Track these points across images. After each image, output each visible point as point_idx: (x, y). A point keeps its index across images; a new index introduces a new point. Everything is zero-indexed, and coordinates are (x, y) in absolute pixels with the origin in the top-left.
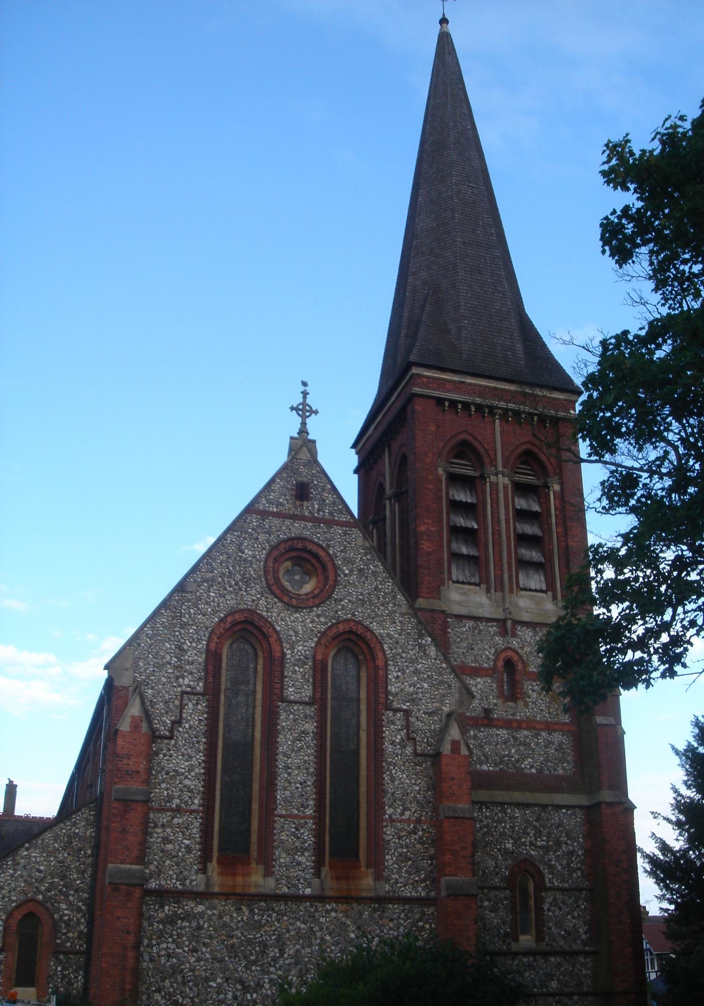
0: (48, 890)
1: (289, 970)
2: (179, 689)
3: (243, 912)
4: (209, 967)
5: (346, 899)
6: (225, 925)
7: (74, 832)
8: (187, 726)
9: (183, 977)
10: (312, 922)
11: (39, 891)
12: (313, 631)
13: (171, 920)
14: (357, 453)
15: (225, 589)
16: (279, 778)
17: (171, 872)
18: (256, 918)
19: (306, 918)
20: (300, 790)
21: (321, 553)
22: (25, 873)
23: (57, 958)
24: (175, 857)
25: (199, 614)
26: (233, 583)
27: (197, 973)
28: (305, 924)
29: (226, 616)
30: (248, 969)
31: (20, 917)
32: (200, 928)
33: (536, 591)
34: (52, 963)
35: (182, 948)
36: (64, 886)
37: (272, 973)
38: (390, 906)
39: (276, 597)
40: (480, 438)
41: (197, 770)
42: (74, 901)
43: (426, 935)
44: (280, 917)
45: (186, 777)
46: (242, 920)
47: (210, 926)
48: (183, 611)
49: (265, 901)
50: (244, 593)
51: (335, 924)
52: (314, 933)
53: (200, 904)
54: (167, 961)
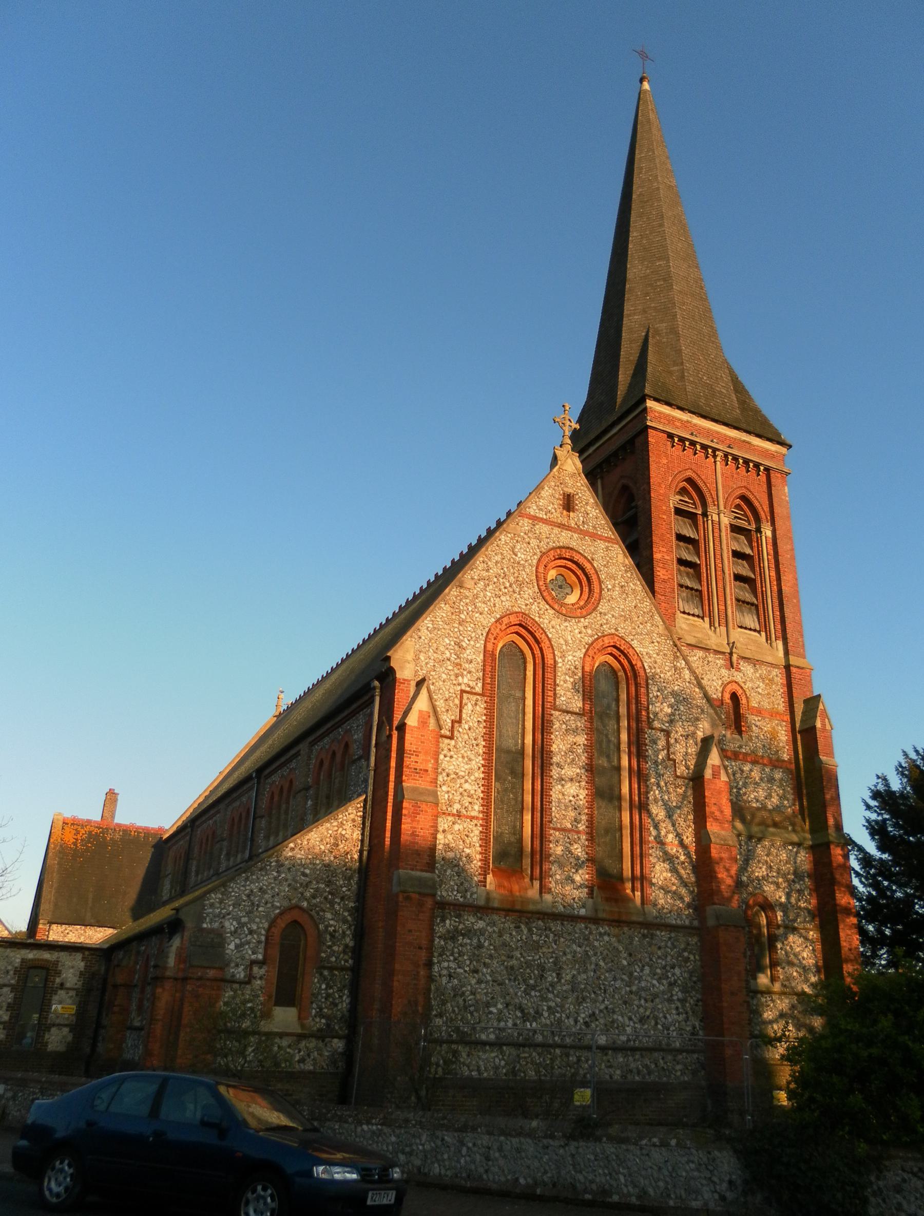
0: (314, 897)
1: (567, 998)
2: (459, 688)
3: (522, 931)
4: (490, 991)
5: (617, 922)
6: (505, 944)
7: (340, 834)
8: (467, 727)
9: (464, 1000)
10: (587, 946)
11: (303, 897)
12: (581, 641)
13: (452, 936)
15: (500, 590)
16: (553, 790)
17: (452, 883)
18: (535, 937)
19: (581, 941)
20: (573, 803)
21: (587, 566)
22: (289, 876)
23: (321, 974)
24: (456, 866)
25: (477, 613)
26: (508, 585)
27: (478, 997)
28: (580, 947)
29: (502, 617)
30: (528, 994)
31: (283, 926)
32: (480, 946)
33: (750, 629)
34: (316, 980)
35: (463, 968)
36: (330, 893)
37: (550, 1000)
38: (658, 933)
39: (548, 603)
40: (703, 477)
41: (477, 775)
42: (339, 911)
43: (691, 967)
44: (557, 938)
45: (466, 781)
46: (522, 939)
47: (491, 944)
48: (461, 608)
49: (542, 920)
50: (518, 596)
51: (608, 949)
52: (589, 957)
53: (481, 919)
54: (448, 982)
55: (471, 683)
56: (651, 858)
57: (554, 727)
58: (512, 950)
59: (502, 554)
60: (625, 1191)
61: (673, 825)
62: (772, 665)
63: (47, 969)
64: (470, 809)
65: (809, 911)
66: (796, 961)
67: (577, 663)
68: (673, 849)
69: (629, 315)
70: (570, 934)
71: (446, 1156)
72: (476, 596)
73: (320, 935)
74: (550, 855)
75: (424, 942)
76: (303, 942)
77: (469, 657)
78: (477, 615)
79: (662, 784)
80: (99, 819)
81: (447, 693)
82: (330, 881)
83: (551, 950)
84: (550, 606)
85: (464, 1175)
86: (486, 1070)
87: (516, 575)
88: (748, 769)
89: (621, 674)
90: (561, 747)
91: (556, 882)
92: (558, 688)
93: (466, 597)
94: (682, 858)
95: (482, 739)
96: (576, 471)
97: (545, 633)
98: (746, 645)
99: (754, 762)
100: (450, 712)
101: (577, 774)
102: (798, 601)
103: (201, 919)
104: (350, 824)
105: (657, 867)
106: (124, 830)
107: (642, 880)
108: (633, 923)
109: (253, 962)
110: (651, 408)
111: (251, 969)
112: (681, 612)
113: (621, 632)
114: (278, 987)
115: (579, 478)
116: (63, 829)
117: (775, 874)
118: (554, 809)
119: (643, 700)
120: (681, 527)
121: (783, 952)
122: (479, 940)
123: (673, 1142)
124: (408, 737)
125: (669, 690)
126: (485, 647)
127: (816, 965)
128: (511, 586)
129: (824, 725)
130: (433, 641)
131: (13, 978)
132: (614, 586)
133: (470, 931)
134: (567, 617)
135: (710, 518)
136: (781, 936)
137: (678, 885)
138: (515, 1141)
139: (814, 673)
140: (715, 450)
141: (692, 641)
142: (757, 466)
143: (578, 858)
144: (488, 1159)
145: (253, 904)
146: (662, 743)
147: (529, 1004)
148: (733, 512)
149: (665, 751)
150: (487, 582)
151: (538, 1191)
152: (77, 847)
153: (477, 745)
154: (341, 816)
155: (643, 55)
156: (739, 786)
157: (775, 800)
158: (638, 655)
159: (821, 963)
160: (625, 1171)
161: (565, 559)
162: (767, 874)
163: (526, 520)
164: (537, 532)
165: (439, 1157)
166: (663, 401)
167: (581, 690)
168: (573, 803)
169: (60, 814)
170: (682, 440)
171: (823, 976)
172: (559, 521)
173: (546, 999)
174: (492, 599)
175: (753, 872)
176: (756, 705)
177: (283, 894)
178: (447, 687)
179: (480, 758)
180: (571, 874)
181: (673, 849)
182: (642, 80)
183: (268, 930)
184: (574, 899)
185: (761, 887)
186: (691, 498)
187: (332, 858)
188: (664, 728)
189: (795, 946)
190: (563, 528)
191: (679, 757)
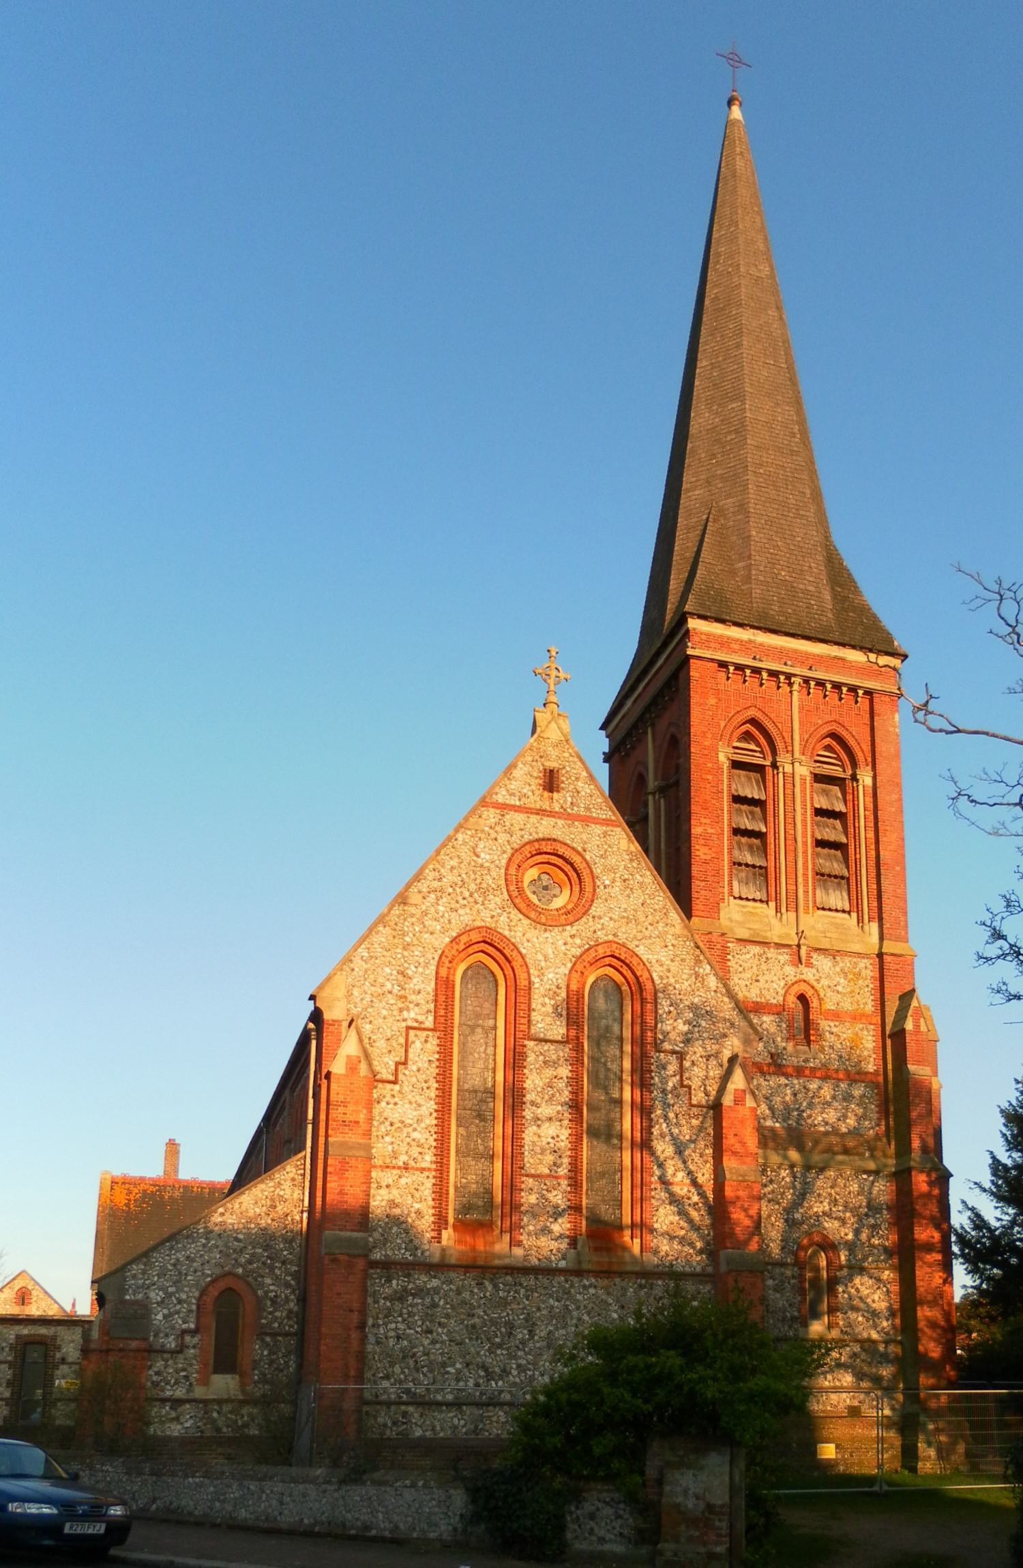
0: (250, 1262)
2: (404, 1024)
5: (606, 1273)
6: (464, 1302)
8: (415, 1068)
9: (416, 1362)
10: (567, 1299)
12: (566, 954)
13: (400, 1297)
14: (607, 737)
15: (457, 902)
16: (527, 1132)
17: (398, 1241)
21: (576, 859)
22: (220, 1243)
23: (263, 1340)
26: (467, 894)
27: (432, 1357)
29: (459, 935)
31: (216, 1294)
32: (434, 1305)
33: (837, 911)
35: (414, 1329)
36: (268, 1257)
40: (772, 716)
45: (415, 1130)
46: (485, 1297)
47: (447, 1303)
48: (406, 929)
49: (511, 1274)
50: (482, 907)
51: (594, 1303)
53: (435, 1277)
55: (420, 1018)
56: (653, 1201)
57: (528, 1060)
58: (473, 1307)
59: (459, 857)
60: (382, 1526)
61: (684, 1162)
62: (859, 955)
63: (46, 1344)
64: (420, 1160)
65: (886, 1249)
66: (862, 1305)
67: (560, 981)
68: (682, 1188)
69: (688, 490)
70: (545, 1288)
71: (250, 1502)
72: (425, 913)
73: (259, 1301)
74: (522, 1205)
75: (356, 1305)
76: (241, 1309)
77: (417, 988)
78: (426, 936)
79: (671, 1115)
80: (161, 1173)
81: (389, 1031)
82: (267, 1246)
83: (521, 1306)
84: (524, 915)
85: (263, 1518)
86: (442, 1429)
87: (478, 881)
88: (815, 1086)
89: (625, 988)
90: (537, 1082)
91: (529, 1234)
92: (533, 1014)
93: (412, 916)
94: (695, 1198)
95: (434, 1080)
96: (563, 738)
97: (518, 949)
98: (824, 932)
99: (825, 1078)
100: (393, 1053)
101: (558, 1112)
102: (904, 869)
103: (123, 1291)
104: (289, 1183)
105: (660, 1210)
106: (185, 1187)
107: (642, 1227)
108: (627, 1273)
109: (184, 1332)
110: (694, 629)
111: (183, 1339)
112: (735, 898)
113: (622, 938)
114: (216, 1354)
115: (567, 746)
116: (112, 1189)
117: (840, 1208)
118: (526, 1153)
119: (650, 1019)
120: (743, 786)
121: (846, 1296)
122: (432, 1299)
123: (420, 1483)
124: (333, 1086)
125: (687, 1003)
126: (437, 973)
127: (890, 1309)
128: (471, 895)
129: (917, 1026)
130: (369, 972)
131: (9, 1355)
132: (613, 881)
133: (422, 1290)
134: (547, 926)
135: (781, 769)
136: (845, 1277)
137: (688, 1229)
138: (301, 1487)
139: (916, 960)
140: (789, 676)
141: (743, 933)
142: (853, 689)
143: (556, 1207)
144: (281, 1503)
145: (180, 1273)
146: (672, 1068)
147: (495, 1363)
148: (816, 761)
149: (678, 1077)
150: (439, 894)
151: (317, 1529)
152: (130, 1209)
153: (428, 1088)
154: (277, 1176)
155: (734, 60)
156: (802, 1108)
157: (851, 1121)
158: (644, 964)
159: (896, 1306)
160: (383, 1510)
161: (546, 853)
162: (831, 1209)
163: (492, 810)
164: (508, 824)
165: (246, 1503)
166: (711, 617)
167: (564, 1013)
168: (552, 1145)
169: (107, 1172)
170: (740, 668)
171: (898, 1321)
172: (538, 807)
173: (516, 1357)
174: (446, 915)
175: (811, 1207)
176: (833, 1008)
177: (214, 1261)
178: (389, 1025)
179: (432, 1102)
180: (548, 1224)
181: (682, 1188)
182: (730, 103)
183: (199, 1299)
184: (551, 1251)
185: (821, 1223)
186: (758, 745)
187: (269, 1221)
188: (677, 1049)
189: (862, 1289)
190: (543, 815)
191: (695, 1083)
